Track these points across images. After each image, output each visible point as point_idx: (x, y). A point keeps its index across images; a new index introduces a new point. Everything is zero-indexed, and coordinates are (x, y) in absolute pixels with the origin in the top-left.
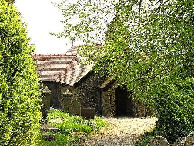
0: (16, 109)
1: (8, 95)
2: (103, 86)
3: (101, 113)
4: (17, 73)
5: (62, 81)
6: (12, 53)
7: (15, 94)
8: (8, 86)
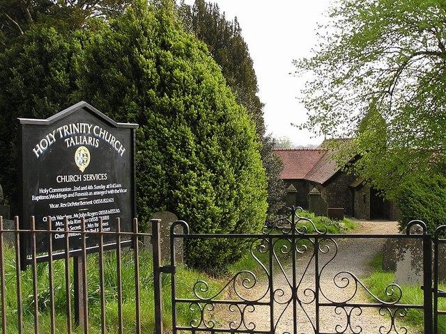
0: (242, 199)
1: (235, 186)
2: (355, 185)
3: (352, 214)
4: (243, 167)
5: (311, 179)
6: (239, 149)
7: (242, 186)
8: (236, 178)
